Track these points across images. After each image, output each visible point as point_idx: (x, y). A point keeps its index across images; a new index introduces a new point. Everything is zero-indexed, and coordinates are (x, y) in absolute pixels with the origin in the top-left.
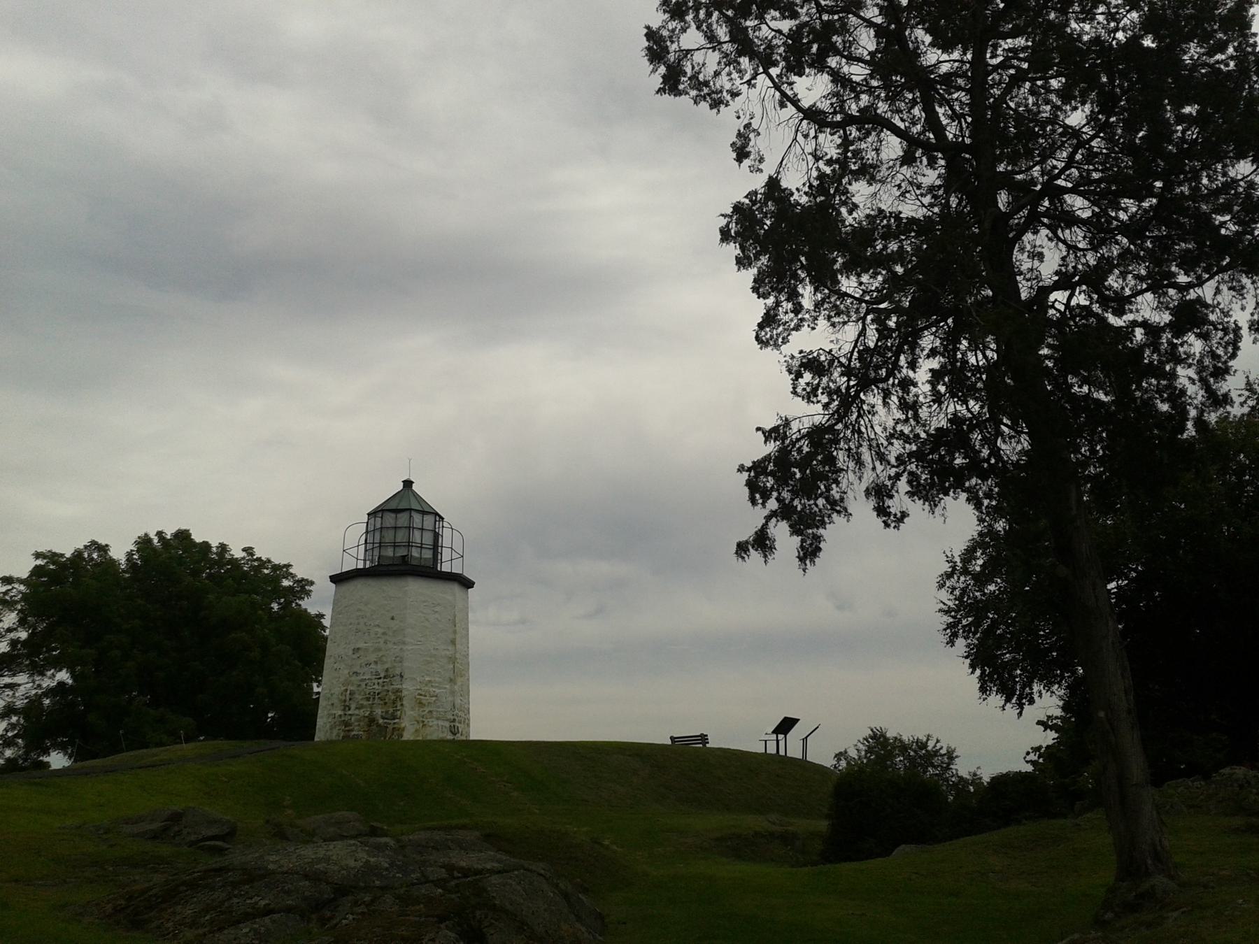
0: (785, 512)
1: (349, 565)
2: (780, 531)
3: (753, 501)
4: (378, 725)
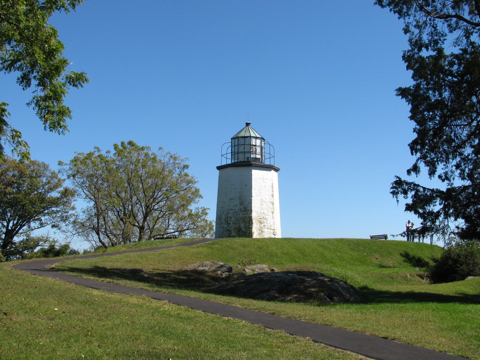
0: (423, 157)
1: (224, 163)
2: (422, 165)
3: (412, 154)
4: (243, 231)
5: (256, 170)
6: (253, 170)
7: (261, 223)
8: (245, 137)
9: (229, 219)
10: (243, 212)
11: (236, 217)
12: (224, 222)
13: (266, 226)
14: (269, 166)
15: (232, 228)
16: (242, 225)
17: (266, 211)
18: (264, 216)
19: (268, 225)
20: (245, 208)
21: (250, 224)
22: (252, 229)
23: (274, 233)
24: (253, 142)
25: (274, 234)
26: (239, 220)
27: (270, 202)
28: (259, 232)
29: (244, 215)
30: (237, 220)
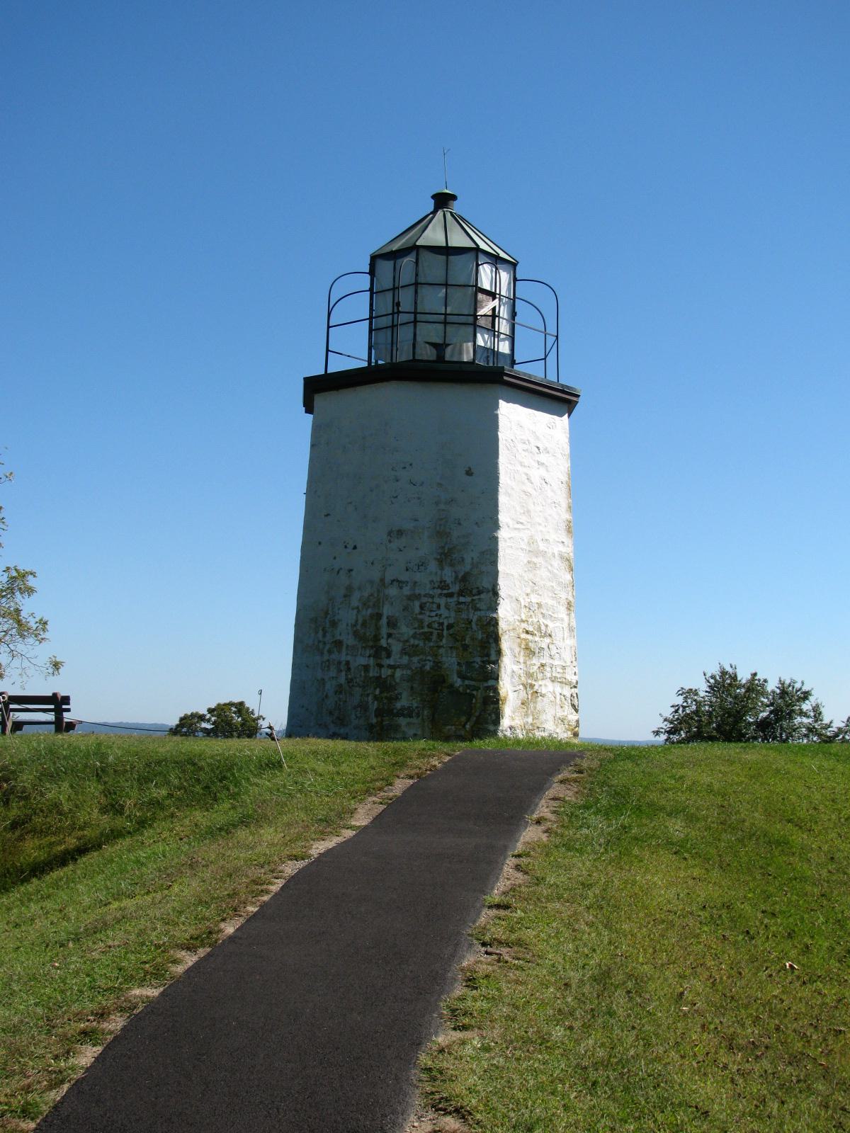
4: (453, 690)
5: (511, 405)
6: (502, 403)
7: (530, 652)
8: (448, 251)
9: (384, 631)
10: (453, 600)
11: (421, 621)
12: (350, 640)
13: (548, 669)
14: (563, 392)
15: (398, 673)
16: (450, 661)
17: (547, 600)
18: (542, 620)
19: (556, 662)
20: (465, 578)
21: (488, 655)
22: (497, 678)
23: (576, 702)
24: (486, 276)
25: (573, 706)
26: (434, 637)
27: (562, 557)
28: (523, 694)
29: (459, 611)
30: (427, 637)
